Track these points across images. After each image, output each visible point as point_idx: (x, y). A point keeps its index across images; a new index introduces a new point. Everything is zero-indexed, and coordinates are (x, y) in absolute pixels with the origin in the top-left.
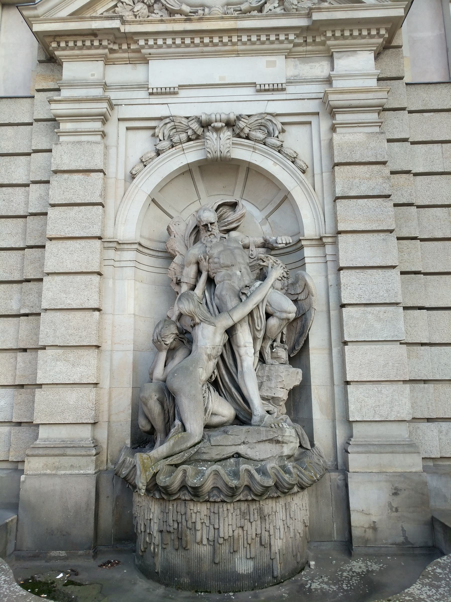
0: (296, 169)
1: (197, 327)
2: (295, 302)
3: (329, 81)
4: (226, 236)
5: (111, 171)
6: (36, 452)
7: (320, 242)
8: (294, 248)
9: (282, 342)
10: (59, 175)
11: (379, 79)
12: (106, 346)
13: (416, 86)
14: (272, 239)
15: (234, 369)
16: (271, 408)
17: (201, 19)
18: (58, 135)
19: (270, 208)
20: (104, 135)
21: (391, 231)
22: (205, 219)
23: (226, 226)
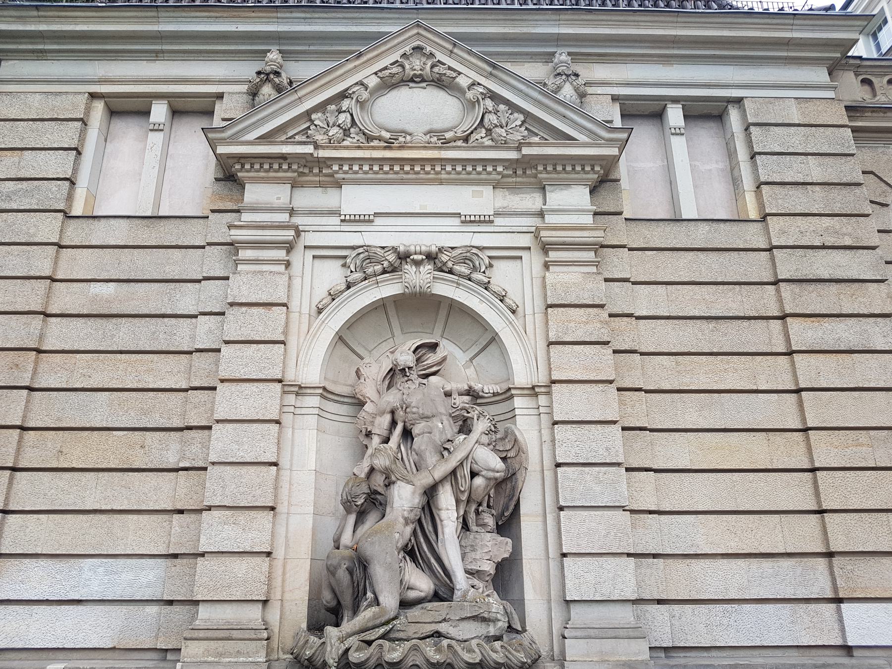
0: (505, 308)
1: (392, 486)
2: (504, 459)
3: (541, 214)
4: (425, 381)
5: (294, 305)
6: (196, 634)
7: (532, 391)
8: (503, 397)
9: (489, 506)
10: (236, 308)
11: (596, 214)
12: (282, 508)
13: (637, 222)
14: (478, 387)
15: (434, 537)
16: (476, 582)
17: (401, 148)
18: (236, 263)
19: (475, 350)
20: (288, 264)
21: (611, 382)
22: (403, 363)
23: (425, 370)
